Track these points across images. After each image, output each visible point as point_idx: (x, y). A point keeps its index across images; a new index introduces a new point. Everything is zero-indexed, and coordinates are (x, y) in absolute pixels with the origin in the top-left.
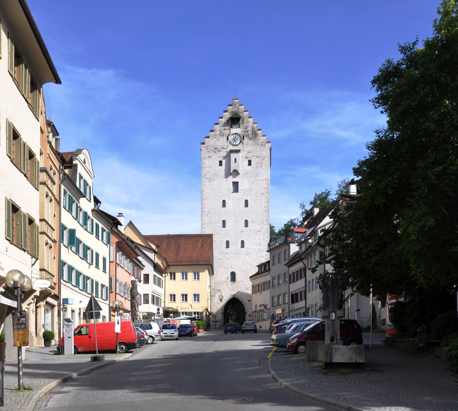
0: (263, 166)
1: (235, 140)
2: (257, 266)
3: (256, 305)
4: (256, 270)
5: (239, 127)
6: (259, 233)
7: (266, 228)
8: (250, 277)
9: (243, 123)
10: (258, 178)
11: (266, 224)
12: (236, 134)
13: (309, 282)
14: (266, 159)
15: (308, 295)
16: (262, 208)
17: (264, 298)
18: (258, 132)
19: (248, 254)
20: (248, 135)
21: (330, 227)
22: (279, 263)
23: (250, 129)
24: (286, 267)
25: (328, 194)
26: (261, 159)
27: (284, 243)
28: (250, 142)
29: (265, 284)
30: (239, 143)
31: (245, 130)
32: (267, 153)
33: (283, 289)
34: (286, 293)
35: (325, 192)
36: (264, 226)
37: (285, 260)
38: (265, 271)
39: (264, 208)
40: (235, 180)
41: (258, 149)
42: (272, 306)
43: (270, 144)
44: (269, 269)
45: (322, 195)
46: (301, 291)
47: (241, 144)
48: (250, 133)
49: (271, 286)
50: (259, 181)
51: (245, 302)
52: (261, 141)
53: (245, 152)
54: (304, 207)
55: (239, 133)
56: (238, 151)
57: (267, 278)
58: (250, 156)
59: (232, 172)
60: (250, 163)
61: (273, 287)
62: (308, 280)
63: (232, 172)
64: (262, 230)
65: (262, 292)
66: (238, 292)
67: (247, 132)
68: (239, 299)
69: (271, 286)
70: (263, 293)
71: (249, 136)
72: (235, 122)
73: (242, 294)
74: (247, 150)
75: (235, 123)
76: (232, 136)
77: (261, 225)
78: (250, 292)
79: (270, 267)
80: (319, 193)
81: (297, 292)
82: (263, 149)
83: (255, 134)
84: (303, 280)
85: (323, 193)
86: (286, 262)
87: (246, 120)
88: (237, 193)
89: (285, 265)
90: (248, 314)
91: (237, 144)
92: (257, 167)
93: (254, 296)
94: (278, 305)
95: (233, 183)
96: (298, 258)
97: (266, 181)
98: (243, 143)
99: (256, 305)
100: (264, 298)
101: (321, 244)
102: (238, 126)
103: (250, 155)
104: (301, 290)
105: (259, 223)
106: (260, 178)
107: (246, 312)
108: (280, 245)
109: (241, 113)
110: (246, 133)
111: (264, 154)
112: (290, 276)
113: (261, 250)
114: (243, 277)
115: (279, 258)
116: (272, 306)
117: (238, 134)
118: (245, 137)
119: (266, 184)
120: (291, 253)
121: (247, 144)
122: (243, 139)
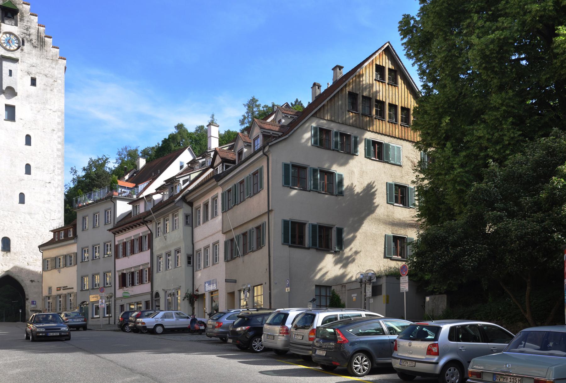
0: (55, 90)
1: (8, 42)
2: (52, 231)
3: (50, 289)
4: (51, 236)
5: (16, 25)
6: (48, 185)
7: (59, 180)
8: (40, 247)
9: (22, 20)
10: (46, 106)
11: (59, 175)
12: (10, 33)
13: (159, 257)
14: (59, 81)
15: (157, 277)
16: (53, 151)
17: (67, 278)
18: (46, 39)
19: (30, 214)
20: (31, 40)
21: (145, 189)
22: (83, 230)
23: (33, 31)
24: (111, 234)
25: (106, 161)
26: (51, 81)
27: (106, 198)
28: (34, 51)
29: (68, 258)
30: (16, 48)
31: (25, 31)
32: (60, 73)
33: (104, 265)
34: (110, 272)
35: (102, 158)
36: (56, 177)
37: (105, 224)
38: (67, 238)
39: (55, 150)
40: (11, 102)
41: (47, 65)
42: (82, 290)
43: (65, 61)
44: (75, 236)
45: (98, 161)
46: (142, 270)
47: (19, 50)
48: (34, 37)
49: (79, 260)
50: (49, 112)
51: (26, 284)
52: (51, 53)
53: (25, 64)
54: (76, 172)
55: (16, 34)
56: (15, 60)
57: (72, 248)
58: (33, 72)
59: (4, 88)
60: (33, 82)
61: (82, 262)
62: (156, 254)
63: (4, 88)
64: (52, 182)
65: (62, 269)
66: (15, 267)
67: (29, 35)
68: (16, 278)
69: (79, 260)
70: (63, 270)
71: (33, 42)
72: (9, 15)
73: (21, 270)
74: (29, 62)
75: (10, 18)
76: (4, 36)
77: (51, 175)
78: (37, 267)
79: (78, 234)
80: (95, 158)
81: (133, 270)
82: (54, 66)
83: (41, 43)
84: (147, 253)
85: (99, 159)
86: (111, 226)
87: (27, 16)
88: (13, 123)
89: (110, 230)
90: (30, 301)
91: (12, 49)
92: (45, 90)
93: (46, 274)
94: (93, 289)
95: (7, 106)
96: (128, 222)
97: (59, 113)
98: (22, 50)
99: (50, 289)
100: (67, 278)
101: (188, 201)
102: (13, 22)
103: (33, 71)
104: (141, 268)
105: (48, 170)
106: (50, 108)
107: (27, 297)
108: (96, 202)
109: (19, 4)
110: (28, 37)
111: (56, 73)
112: (116, 247)
113: (52, 211)
114: (23, 246)
115: (94, 221)
116: (82, 290)
117: (15, 36)
118: (26, 43)
119: (59, 117)
120: (118, 216)
121: (29, 54)
122: (23, 44)
